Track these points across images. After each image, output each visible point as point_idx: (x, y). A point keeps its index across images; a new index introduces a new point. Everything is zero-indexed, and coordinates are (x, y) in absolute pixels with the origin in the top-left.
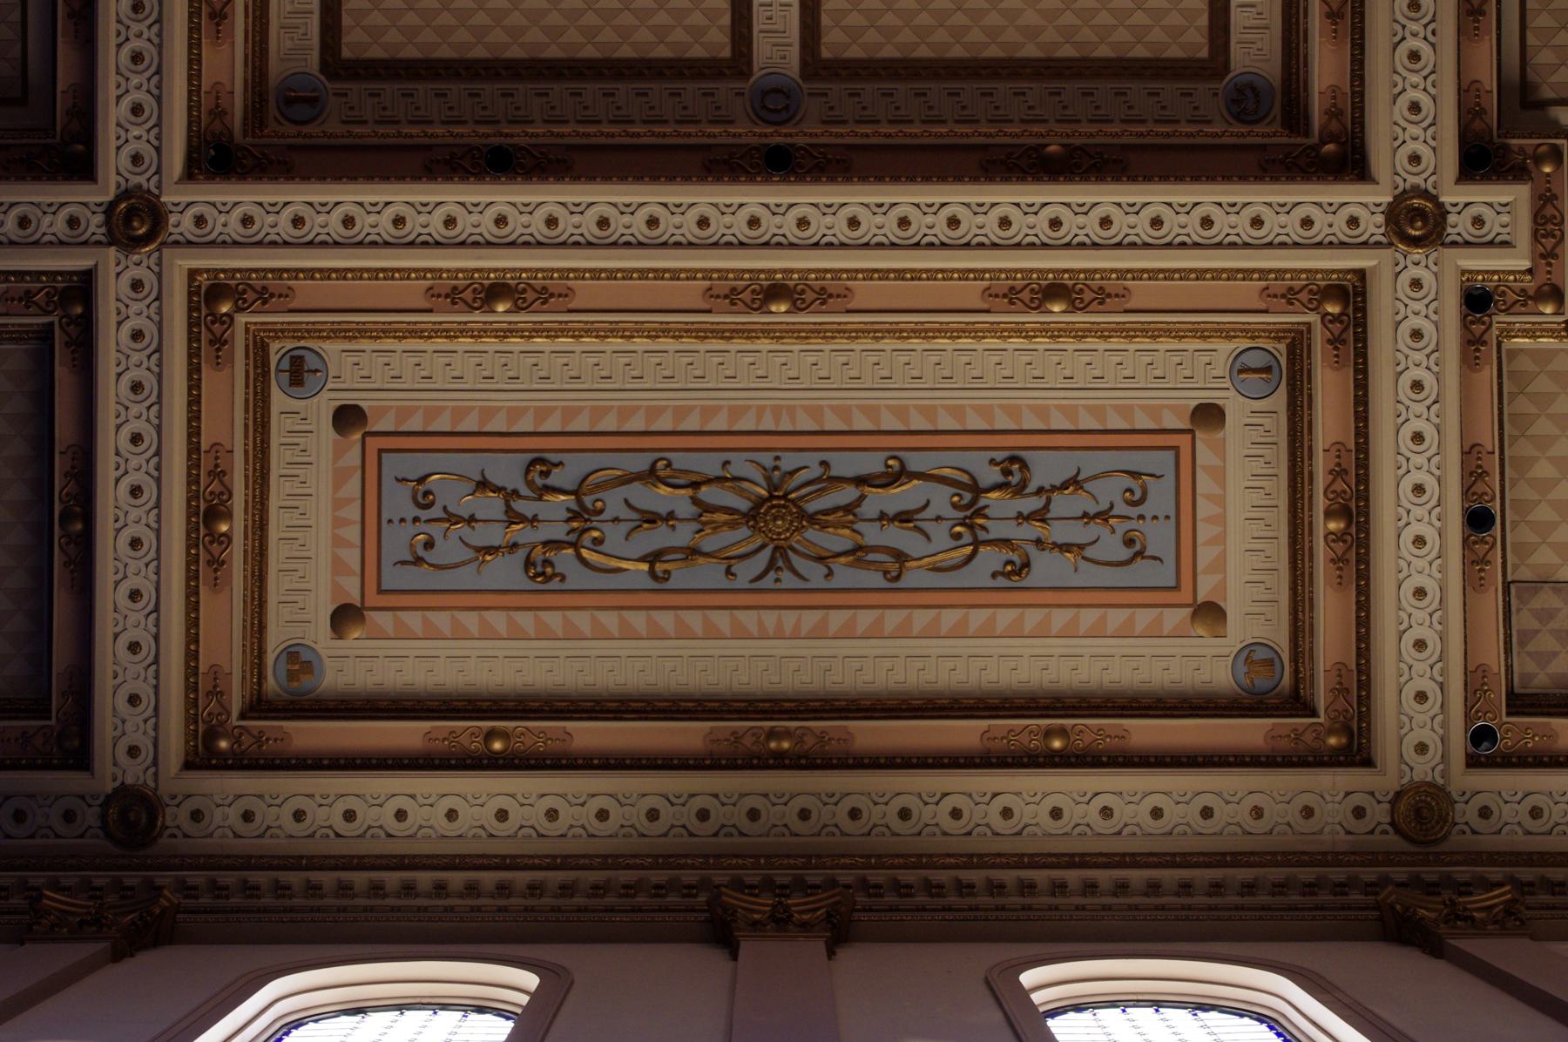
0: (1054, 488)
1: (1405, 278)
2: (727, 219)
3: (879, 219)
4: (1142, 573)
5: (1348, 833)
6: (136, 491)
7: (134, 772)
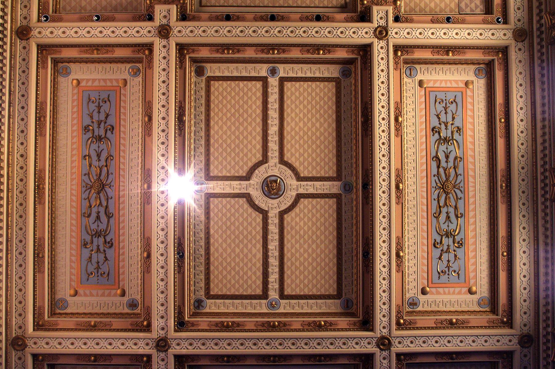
0: (439, 121)
1: (395, 36)
2: (383, 199)
3: (383, 162)
4: (459, 100)
5: (524, 52)
6: (449, 342)
7: (515, 340)
